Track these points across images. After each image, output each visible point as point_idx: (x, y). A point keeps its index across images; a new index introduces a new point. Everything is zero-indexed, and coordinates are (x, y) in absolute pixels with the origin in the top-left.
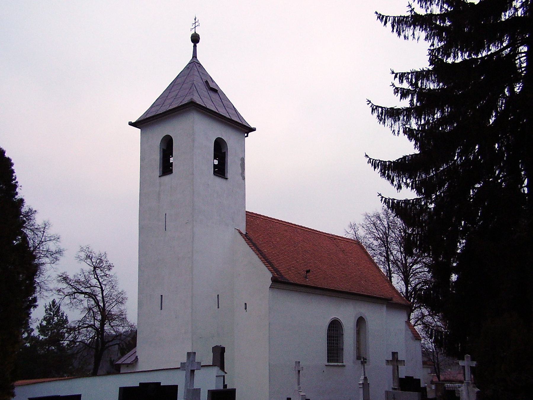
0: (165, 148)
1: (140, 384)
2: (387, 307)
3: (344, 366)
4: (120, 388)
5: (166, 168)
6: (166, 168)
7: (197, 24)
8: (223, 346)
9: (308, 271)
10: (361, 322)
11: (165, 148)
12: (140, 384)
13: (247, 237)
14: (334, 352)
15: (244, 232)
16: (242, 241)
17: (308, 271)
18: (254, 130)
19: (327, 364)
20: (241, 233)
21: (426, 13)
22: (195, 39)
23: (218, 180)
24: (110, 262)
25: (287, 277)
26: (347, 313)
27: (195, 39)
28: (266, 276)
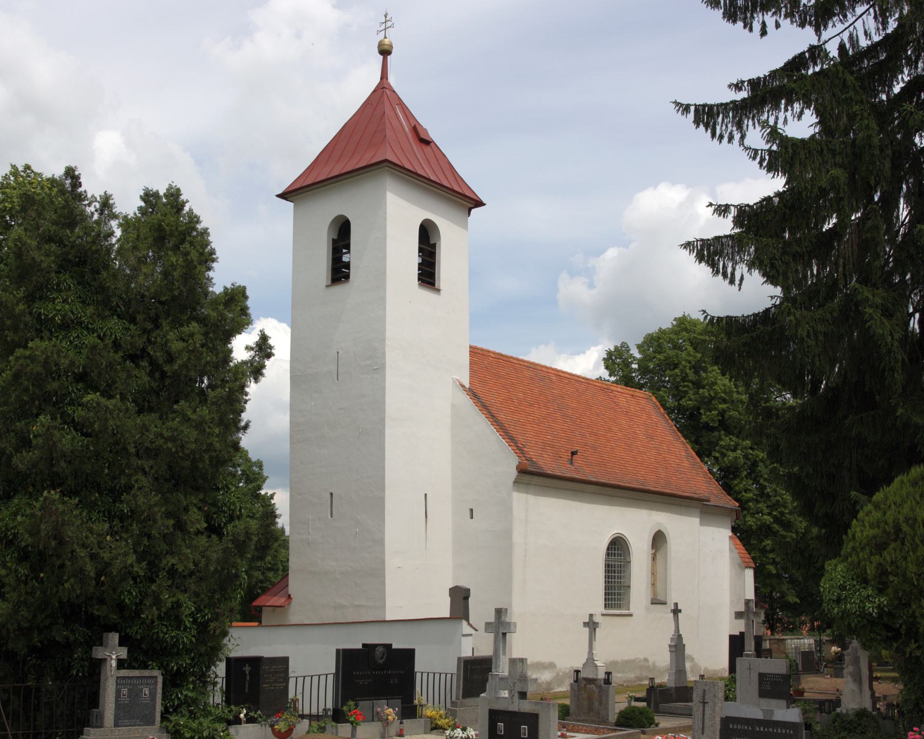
0: (336, 238)
1: (364, 645)
2: (701, 512)
3: (631, 615)
4: (338, 651)
5: (339, 272)
6: (339, 272)
7: (389, 24)
8: (467, 586)
9: (573, 453)
10: (659, 540)
11: (336, 238)
12: (364, 645)
13: (472, 393)
14: (616, 591)
15: (467, 386)
16: (466, 401)
17: (573, 453)
18: (484, 204)
19: (605, 612)
20: (463, 386)
21: (869, 43)
22: (385, 52)
23: (426, 294)
24: (642, 658)
25: (541, 463)
26: (636, 523)
27: (385, 52)
28: (509, 463)
